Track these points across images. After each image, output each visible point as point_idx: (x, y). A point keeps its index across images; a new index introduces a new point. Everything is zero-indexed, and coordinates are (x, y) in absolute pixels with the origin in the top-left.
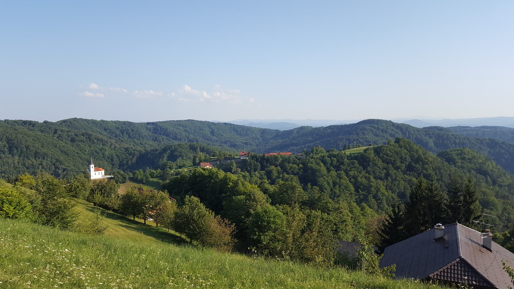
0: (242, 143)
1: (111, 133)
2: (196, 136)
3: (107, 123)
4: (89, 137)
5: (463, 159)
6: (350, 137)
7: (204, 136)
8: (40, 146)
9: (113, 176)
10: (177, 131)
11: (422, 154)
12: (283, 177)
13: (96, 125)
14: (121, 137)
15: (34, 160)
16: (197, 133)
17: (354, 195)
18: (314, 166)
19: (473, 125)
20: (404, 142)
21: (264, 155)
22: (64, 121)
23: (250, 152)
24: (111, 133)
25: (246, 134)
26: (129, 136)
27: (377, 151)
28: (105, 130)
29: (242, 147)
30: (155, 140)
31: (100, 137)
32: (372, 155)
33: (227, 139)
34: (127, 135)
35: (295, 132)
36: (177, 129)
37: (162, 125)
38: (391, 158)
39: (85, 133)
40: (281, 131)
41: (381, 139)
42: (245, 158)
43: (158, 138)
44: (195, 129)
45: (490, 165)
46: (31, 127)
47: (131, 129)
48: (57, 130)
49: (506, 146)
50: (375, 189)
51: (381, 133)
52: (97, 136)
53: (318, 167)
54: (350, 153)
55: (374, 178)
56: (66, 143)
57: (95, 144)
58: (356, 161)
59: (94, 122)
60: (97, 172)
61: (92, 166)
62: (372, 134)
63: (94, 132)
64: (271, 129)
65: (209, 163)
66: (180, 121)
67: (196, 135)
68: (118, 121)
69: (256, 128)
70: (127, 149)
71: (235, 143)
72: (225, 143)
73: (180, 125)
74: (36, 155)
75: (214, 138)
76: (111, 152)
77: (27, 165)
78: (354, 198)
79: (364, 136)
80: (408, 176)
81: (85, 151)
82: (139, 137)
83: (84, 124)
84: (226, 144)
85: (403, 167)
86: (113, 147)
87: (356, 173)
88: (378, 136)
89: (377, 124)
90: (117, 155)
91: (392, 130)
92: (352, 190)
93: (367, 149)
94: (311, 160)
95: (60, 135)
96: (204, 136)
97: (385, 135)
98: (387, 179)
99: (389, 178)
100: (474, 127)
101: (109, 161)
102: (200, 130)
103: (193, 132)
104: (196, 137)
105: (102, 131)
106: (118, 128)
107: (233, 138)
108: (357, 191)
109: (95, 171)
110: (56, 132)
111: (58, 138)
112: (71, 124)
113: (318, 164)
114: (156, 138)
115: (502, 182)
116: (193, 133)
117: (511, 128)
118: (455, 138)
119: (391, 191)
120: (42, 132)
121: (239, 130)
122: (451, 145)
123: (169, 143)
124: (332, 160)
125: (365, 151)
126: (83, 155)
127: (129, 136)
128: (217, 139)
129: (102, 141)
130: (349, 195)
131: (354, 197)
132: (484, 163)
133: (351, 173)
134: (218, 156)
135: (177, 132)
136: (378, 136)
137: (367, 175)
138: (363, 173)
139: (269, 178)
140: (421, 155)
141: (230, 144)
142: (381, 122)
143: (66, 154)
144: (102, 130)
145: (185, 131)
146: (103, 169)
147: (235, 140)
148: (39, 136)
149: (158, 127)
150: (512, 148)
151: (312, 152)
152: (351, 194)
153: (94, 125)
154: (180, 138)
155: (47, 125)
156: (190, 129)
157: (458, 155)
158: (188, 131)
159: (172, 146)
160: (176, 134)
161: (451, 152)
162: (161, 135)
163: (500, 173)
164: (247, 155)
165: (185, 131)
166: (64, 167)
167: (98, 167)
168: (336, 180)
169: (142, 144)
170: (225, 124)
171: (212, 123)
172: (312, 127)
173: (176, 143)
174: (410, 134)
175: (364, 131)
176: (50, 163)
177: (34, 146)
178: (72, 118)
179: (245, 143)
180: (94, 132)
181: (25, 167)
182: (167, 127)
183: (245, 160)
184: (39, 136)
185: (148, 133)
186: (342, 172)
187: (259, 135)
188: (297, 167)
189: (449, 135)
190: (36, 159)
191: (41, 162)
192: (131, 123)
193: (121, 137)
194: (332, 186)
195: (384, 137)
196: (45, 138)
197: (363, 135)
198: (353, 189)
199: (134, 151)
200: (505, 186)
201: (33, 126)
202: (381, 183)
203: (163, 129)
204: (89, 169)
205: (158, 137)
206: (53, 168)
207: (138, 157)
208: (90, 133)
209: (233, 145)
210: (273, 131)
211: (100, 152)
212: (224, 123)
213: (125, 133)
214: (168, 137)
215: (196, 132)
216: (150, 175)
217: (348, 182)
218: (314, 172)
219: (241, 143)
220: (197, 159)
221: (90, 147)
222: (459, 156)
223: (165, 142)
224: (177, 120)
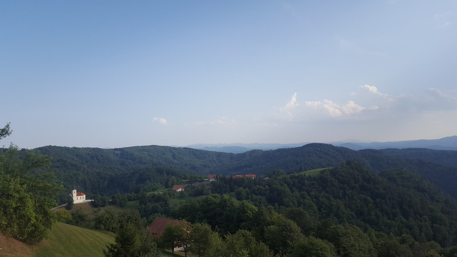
0: (201, 165)
1: (83, 159)
3: (79, 150)
9: (93, 200)
10: (142, 156)
11: (371, 175)
12: (252, 198)
13: (69, 151)
17: (318, 214)
19: (401, 147)
21: (231, 177)
22: (40, 149)
23: (218, 175)
24: (83, 159)
27: (333, 173)
28: (77, 156)
33: (187, 162)
35: (248, 155)
36: (142, 154)
40: (235, 154)
43: (125, 163)
44: (158, 154)
47: (101, 155)
50: (336, 208)
51: (324, 155)
54: (309, 175)
55: (334, 197)
56: (42, 169)
58: (315, 182)
60: (79, 197)
61: (75, 192)
64: (226, 152)
66: (144, 146)
67: (159, 159)
69: (212, 151)
73: (144, 150)
75: (176, 161)
76: (84, 176)
78: (318, 216)
81: (60, 176)
82: (108, 162)
87: (317, 193)
90: (90, 180)
100: (401, 149)
106: (89, 154)
107: (192, 161)
108: (319, 210)
109: (77, 196)
113: (282, 185)
117: (433, 150)
119: (349, 209)
125: (322, 172)
128: (178, 162)
131: (318, 216)
135: (142, 157)
137: (327, 195)
140: (371, 176)
146: (85, 194)
147: (194, 163)
149: (124, 153)
152: (315, 212)
156: (154, 154)
159: (140, 170)
160: (141, 158)
165: (150, 155)
168: (299, 200)
170: (185, 148)
171: (173, 148)
172: (262, 151)
179: (203, 165)
182: (133, 152)
183: (215, 181)
186: (305, 193)
187: (216, 158)
192: (100, 150)
198: (316, 208)
204: (72, 194)
207: (225, 202)
212: (184, 148)
213: (95, 159)
215: (159, 157)
217: (311, 201)
220: (170, 182)
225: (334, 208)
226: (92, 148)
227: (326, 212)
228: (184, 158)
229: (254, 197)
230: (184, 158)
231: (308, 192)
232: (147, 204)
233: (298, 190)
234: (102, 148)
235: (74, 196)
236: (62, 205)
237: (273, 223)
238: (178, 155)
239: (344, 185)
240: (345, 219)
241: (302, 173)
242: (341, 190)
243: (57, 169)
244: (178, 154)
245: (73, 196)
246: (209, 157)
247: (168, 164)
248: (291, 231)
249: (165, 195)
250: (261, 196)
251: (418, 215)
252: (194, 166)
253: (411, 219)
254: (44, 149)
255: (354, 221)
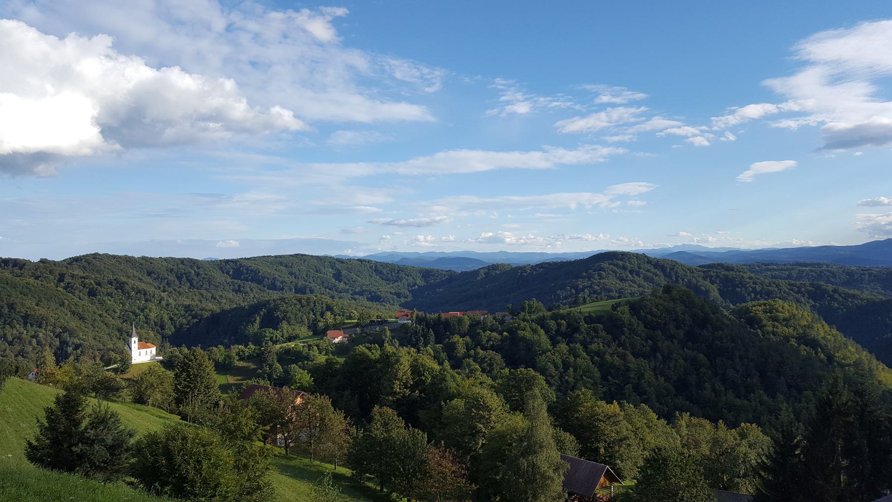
0: (391, 293)
2: (310, 283)
3: (152, 261)
4: (121, 286)
5: (775, 319)
6: (577, 282)
7: (323, 283)
8: (35, 304)
11: (710, 312)
14: (177, 286)
15: (22, 330)
16: (311, 278)
18: (528, 334)
20: (678, 292)
22: (76, 259)
24: (160, 280)
25: (397, 278)
26: (192, 284)
27: (635, 308)
28: (149, 274)
29: (392, 302)
30: (238, 290)
31: (142, 286)
32: (625, 314)
33: (364, 288)
34: (189, 284)
37: (248, 264)
38: (660, 321)
39: (115, 280)
41: (630, 286)
42: (407, 321)
43: (243, 288)
45: (820, 329)
46: (16, 270)
48: (64, 274)
49: (840, 295)
52: (136, 284)
53: (536, 337)
55: (633, 354)
57: (132, 299)
59: (128, 260)
60: (143, 351)
61: (135, 339)
62: (614, 278)
63: (129, 277)
65: (342, 332)
66: (280, 257)
68: (172, 258)
70: (188, 308)
71: (379, 293)
72: (361, 293)
73: (281, 264)
74: (26, 319)
77: (10, 339)
79: (602, 281)
80: (691, 352)
83: (112, 264)
84: (363, 296)
85: (681, 333)
86: (164, 303)
87: (601, 347)
88: (625, 280)
89: (621, 260)
90: (171, 319)
91: (648, 271)
92: (596, 376)
93: (618, 305)
94: (523, 324)
95: (69, 283)
96: (323, 283)
97: (636, 278)
98: (655, 357)
99: (659, 355)
101: (157, 330)
102: (317, 272)
103: (304, 276)
104: (311, 285)
105: (143, 276)
106: (172, 270)
108: (604, 378)
109: (139, 349)
110: (61, 278)
111: (65, 288)
112: (89, 264)
114: (239, 286)
115: (843, 359)
116: (305, 277)
118: (755, 283)
120: (37, 278)
121: (384, 271)
122: (748, 295)
123: (262, 295)
124: (559, 325)
125: (614, 308)
126: (111, 319)
127: (192, 284)
128: (347, 287)
129: (145, 294)
130: (592, 385)
132: (810, 327)
133: (594, 347)
134: (358, 319)
135: (276, 276)
136: (625, 280)
137: (620, 350)
138: (614, 346)
139: (450, 358)
140: (710, 314)
141: (370, 295)
142: (628, 256)
143: (81, 318)
144: (142, 274)
145: (291, 274)
147: (378, 289)
148: (33, 286)
150: (850, 300)
151: (523, 309)
153: (128, 266)
154: (282, 286)
155: (46, 266)
157: (765, 312)
158: (295, 273)
160: (274, 279)
161: (754, 308)
162: (248, 281)
163: (838, 343)
164: (410, 316)
166: (77, 341)
167: (144, 342)
169: (215, 299)
173: (275, 295)
174: (679, 277)
175: (601, 272)
176: (52, 334)
177: (23, 305)
178: (90, 254)
179: (395, 294)
180: (129, 277)
181: (7, 341)
182: (259, 267)
184: (33, 286)
185: (224, 278)
186: (578, 345)
188: (499, 337)
189: (743, 277)
190: (26, 326)
191: (35, 332)
193: (177, 286)
194: (561, 369)
195: (635, 283)
196: (43, 289)
197: (600, 279)
198: (597, 374)
199: (201, 310)
200: (849, 365)
201: (21, 269)
202: (645, 363)
203: (251, 271)
204: (128, 345)
205: (242, 285)
206: (58, 343)
208: (124, 279)
209: (375, 298)
210: (444, 273)
211: (141, 313)
213: (184, 279)
214: (260, 284)
216: (238, 354)
218: (529, 346)
219: (389, 293)
221: (124, 304)
222: (769, 314)
223: (254, 294)
224: (276, 255)
225: (632, 376)
226: (179, 259)
227: (617, 382)
228: (360, 279)
229: (479, 353)
230: (360, 279)
231: (585, 346)
232: (274, 366)
233: (566, 340)
234: (200, 259)
235: (132, 349)
236: (109, 365)
237: (459, 395)
238: (346, 273)
239: (656, 332)
240: (654, 397)
241: (577, 309)
242: (649, 340)
243: (108, 299)
244: (346, 271)
245: (131, 349)
246: (407, 278)
247: (327, 290)
248: (488, 409)
249: (309, 350)
250: (494, 352)
251: (794, 391)
252: (376, 294)
253: (780, 397)
254: (83, 260)
255: (670, 399)
